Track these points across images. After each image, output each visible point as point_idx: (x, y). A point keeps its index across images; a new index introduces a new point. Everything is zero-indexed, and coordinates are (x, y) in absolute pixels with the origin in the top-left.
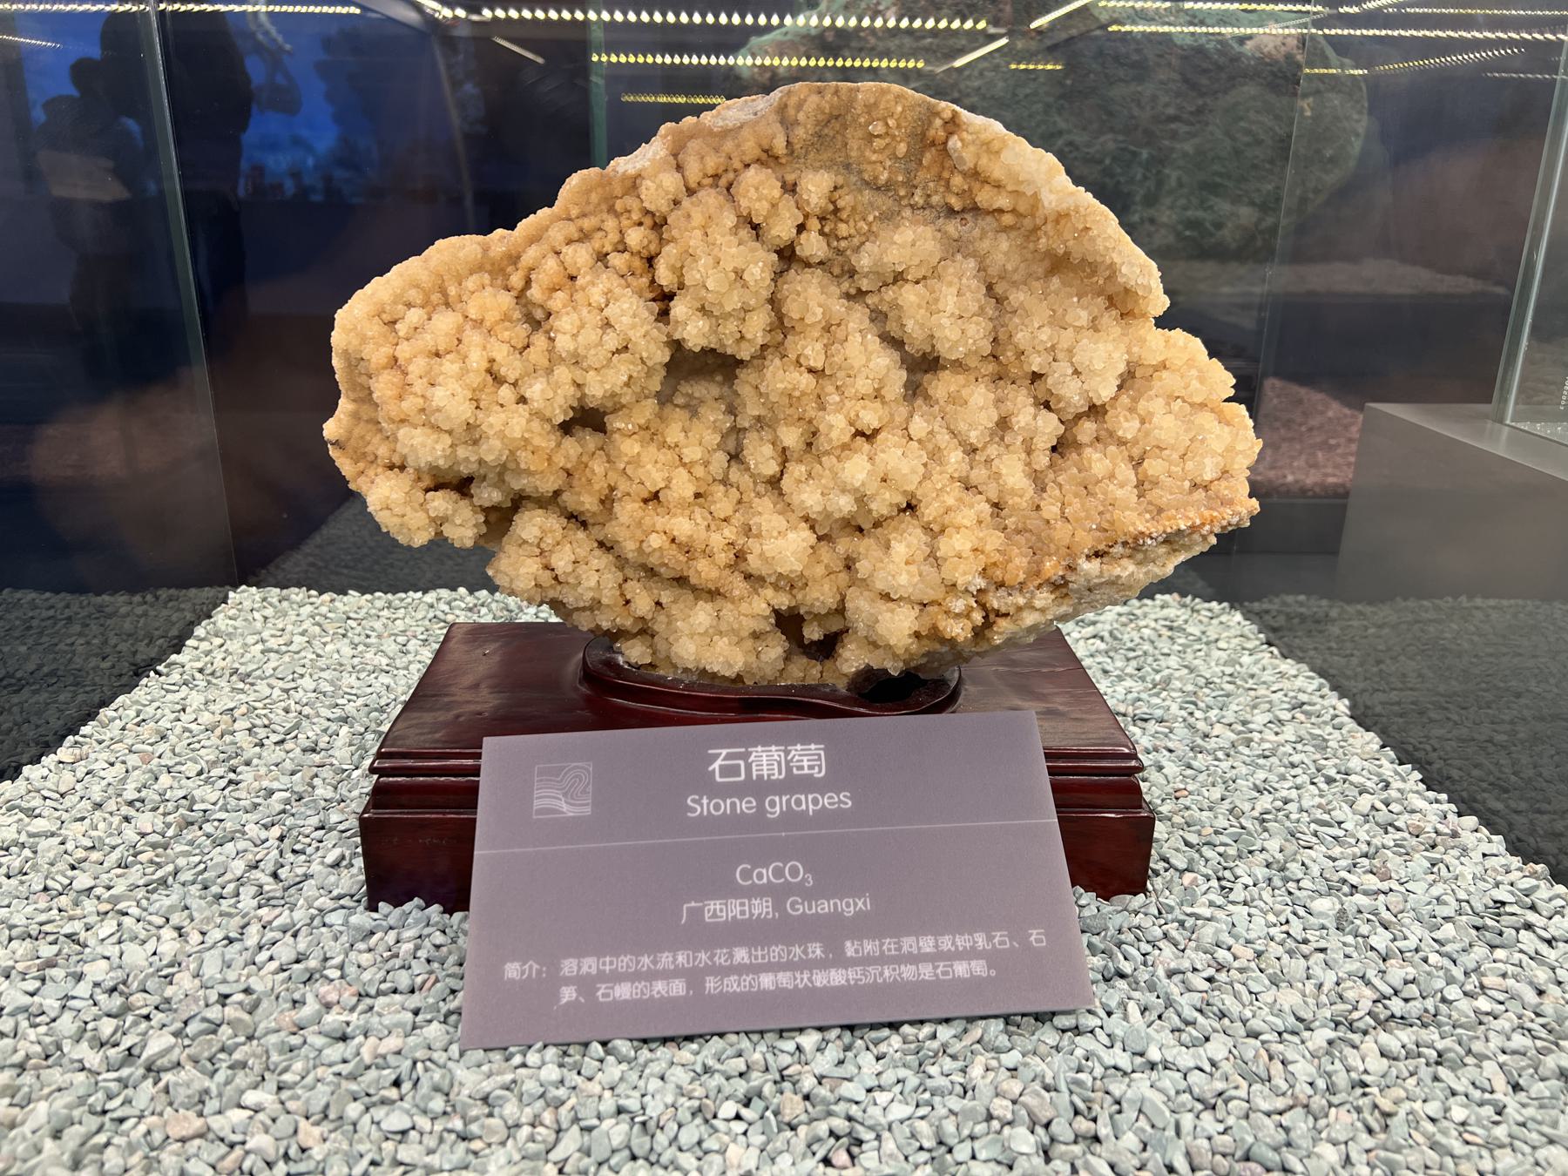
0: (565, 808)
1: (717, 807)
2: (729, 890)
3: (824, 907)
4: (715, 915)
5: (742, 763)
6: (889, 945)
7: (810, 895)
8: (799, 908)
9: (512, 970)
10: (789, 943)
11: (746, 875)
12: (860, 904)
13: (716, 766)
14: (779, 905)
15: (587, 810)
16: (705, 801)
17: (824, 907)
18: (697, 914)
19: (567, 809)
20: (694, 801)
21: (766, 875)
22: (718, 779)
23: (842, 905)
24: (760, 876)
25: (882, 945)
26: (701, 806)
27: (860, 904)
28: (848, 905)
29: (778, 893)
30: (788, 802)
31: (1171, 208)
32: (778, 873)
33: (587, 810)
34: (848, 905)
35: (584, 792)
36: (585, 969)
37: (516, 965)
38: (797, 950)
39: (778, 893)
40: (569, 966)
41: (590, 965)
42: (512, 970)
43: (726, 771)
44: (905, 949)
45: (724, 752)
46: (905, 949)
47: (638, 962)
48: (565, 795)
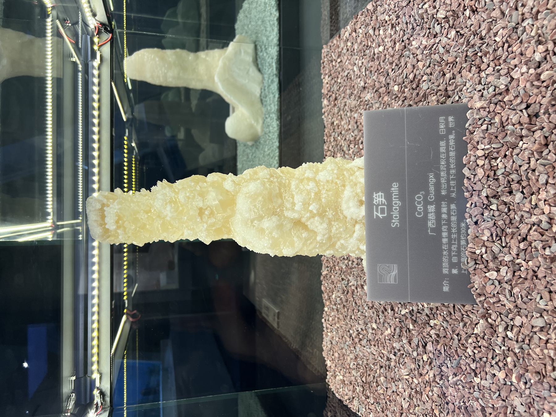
0: (394, 273)
1: (396, 217)
2: (425, 219)
3: (432, 188)
4: (433, 224)
5: (379, 207)
6: (443, 156)
7: (428, 193)
8: (432, 197)
9: (446, 289)
10: (442, 255)
11: (419, 213)
12: (431, 177)
13: (380, 216)
14: (431, 203)
15: (395, 266)
16: (394, 221)
17: (432, 188)
18: (433, 230)
19: (395, 272)
20: (393, 225)
21: (420, 207)
22: (385, 215)
23: (432, 183)
24: (420, 209)
25: (442, 158)
26: (395, 222)
27: (431, 177)
28: (432, 181)
29: (426, 203)
30: (395, 198)
31: (325, 10)
32: (419, 203)
33: (395, 266)
34: (432, 181)
35: (389, 267)
36: (445, 230)
37: (444, 288)
38: (445, 253)
39: (426, 203)
40: (445, 271)
41: (445, 264)
42: (446, 289)
43: (382, 212)
44: (444, 151)
45: (375, 213)
46: (444, 151)
47: (445, 255)
48: (389, 273)
